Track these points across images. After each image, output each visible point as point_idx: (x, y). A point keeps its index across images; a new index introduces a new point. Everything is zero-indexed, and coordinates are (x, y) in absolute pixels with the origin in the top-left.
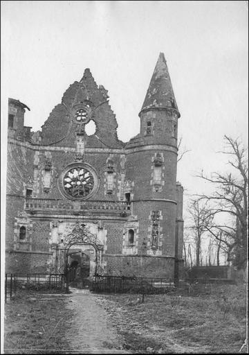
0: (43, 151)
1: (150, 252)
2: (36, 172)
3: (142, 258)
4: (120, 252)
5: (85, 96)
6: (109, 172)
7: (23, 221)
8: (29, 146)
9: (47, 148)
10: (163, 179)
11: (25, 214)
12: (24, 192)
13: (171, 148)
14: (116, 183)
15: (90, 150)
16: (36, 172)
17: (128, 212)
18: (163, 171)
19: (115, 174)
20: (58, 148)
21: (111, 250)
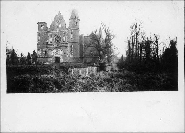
0: (50, 33)
1: (70, 56)
2: (49, 38)
3: (84, 57)
4: (66, 56)
5: (59, 18)
6: (64, 36)
7: (46, 50)
8: (47, 32)
9: (51, 32)
10: (73, 37)
11: (46, 48)
12: (46, 43)
13: (78, 29)
14: (65, 39)
15: (60, 31)
16: (49, 38)
17: (67, 46)
18: (73, 35)
19: (65, 36)
20: (53, 32)
21: (64, 56)
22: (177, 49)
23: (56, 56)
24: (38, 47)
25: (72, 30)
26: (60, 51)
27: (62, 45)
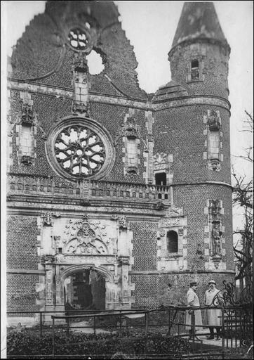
15: (98, 98)
17: (165, 202)
19: (138, 141)
22: (120, 19)
23: (77, 261)
24: (17, 104)
25: (218, 112)
26: (109, 229)
27: (130, 190)
